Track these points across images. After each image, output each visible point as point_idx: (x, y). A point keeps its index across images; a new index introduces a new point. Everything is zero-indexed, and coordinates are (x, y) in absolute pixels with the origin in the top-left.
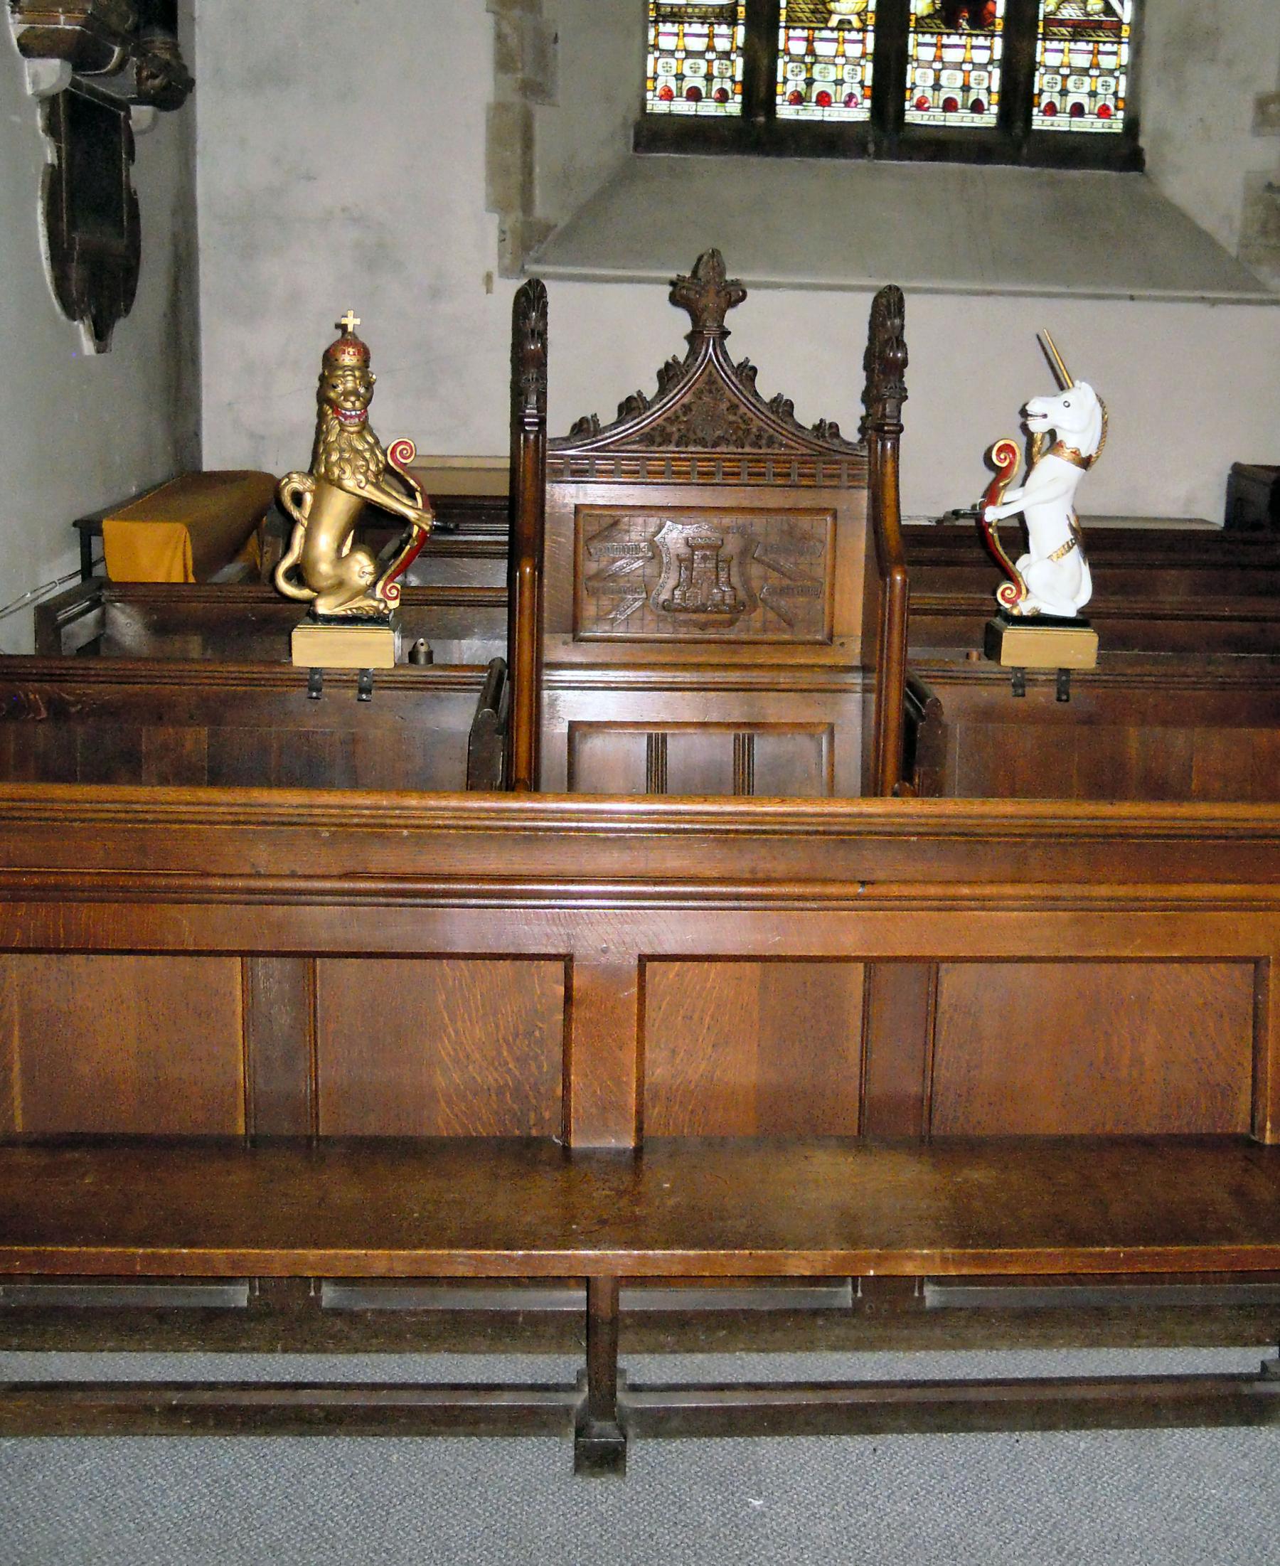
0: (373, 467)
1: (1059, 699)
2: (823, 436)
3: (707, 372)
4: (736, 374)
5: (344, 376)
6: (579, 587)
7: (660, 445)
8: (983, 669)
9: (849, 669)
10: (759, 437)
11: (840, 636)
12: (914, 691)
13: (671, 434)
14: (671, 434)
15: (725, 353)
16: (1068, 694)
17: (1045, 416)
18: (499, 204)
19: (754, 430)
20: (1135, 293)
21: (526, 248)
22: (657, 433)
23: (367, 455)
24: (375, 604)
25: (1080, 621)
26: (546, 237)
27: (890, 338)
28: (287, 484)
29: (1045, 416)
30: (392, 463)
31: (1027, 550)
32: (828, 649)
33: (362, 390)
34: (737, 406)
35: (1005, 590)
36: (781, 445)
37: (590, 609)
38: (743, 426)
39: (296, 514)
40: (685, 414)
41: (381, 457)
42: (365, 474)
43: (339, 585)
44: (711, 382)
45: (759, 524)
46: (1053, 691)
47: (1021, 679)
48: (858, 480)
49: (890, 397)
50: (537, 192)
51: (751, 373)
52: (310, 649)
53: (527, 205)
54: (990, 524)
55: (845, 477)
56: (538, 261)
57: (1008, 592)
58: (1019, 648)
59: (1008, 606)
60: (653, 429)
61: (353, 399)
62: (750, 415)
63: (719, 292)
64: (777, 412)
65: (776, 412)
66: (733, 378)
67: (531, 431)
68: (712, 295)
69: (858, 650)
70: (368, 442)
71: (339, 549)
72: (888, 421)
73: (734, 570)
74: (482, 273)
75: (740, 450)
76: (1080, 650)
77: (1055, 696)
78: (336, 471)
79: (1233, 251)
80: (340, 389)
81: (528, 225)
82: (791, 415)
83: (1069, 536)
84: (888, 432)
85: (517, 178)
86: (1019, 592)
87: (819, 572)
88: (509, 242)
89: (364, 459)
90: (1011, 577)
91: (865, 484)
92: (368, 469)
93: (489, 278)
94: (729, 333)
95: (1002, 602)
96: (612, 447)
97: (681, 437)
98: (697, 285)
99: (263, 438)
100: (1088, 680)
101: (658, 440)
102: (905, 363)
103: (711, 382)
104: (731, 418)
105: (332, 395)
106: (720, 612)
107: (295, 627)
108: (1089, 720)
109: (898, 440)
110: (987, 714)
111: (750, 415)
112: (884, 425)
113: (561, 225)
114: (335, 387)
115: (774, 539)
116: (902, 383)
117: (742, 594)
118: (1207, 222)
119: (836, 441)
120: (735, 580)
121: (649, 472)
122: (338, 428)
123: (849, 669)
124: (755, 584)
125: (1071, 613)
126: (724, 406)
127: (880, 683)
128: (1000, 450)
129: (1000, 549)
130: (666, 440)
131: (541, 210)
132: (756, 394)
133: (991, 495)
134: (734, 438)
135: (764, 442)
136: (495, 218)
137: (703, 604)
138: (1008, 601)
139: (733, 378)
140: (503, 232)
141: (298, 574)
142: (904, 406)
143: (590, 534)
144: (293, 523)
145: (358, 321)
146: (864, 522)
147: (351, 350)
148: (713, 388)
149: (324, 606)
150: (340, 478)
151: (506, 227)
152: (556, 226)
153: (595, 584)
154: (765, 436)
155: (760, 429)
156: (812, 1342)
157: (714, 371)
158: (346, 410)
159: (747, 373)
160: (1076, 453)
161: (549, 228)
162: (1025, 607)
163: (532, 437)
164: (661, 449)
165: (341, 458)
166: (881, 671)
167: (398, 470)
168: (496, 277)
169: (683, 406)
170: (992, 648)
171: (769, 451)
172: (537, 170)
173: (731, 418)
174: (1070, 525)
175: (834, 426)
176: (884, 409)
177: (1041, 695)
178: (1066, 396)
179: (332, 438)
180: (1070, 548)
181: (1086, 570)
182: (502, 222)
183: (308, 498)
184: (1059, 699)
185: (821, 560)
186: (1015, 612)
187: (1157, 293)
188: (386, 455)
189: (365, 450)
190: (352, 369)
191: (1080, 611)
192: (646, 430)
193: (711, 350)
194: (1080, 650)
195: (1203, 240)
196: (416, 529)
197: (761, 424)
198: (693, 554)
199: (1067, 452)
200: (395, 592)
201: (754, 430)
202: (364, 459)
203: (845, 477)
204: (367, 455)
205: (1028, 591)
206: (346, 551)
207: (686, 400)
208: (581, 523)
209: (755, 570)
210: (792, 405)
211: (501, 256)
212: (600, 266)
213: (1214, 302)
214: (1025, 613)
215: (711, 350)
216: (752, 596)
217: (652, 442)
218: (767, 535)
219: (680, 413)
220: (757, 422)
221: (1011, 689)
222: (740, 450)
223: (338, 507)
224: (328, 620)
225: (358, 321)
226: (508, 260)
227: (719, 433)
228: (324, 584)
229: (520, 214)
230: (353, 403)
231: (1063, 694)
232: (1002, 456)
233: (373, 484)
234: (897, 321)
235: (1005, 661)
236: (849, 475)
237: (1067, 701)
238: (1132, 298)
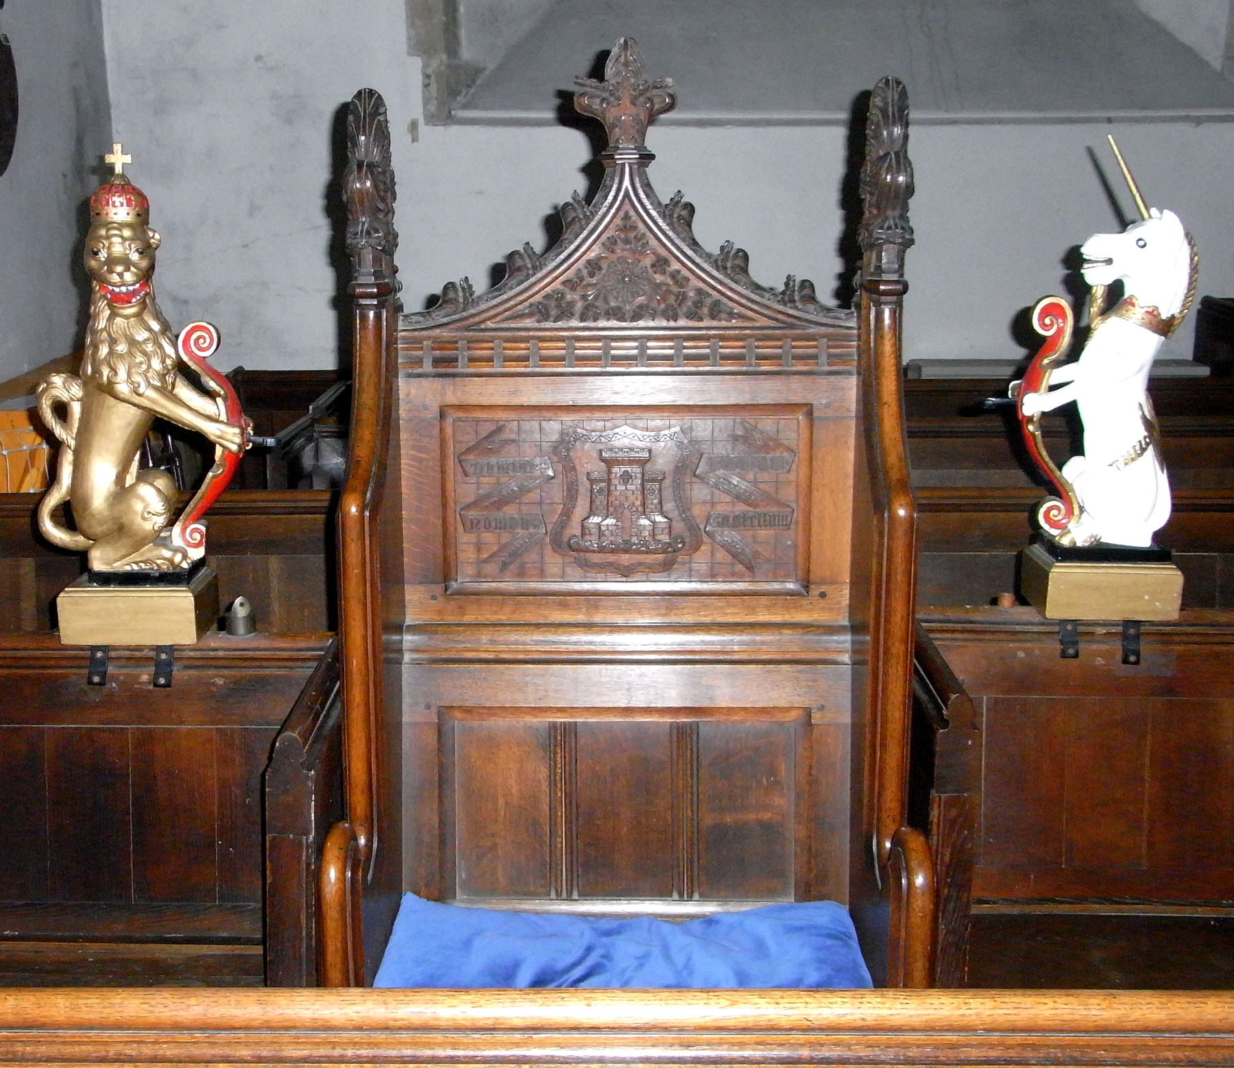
0: (156, 364)
1: (1125, 661)
2: (793, 301)
3: (621, 214)
4: (664, 217)
5: (108, 237)
6: (451, 519)
7: (556, 320)
8: (1016, 618)
9: (832, 630)
10: (698, 304)
11: (823, 582)
12: (927, 666)
13: (572, 304)
14: (572, 304)
15: (647, 186)
16: (1137, 654)
17: (1109, 261)
18: (420, 47)
19: (691, 294)
20: (1112, 114)
21: (453, 93)
22: (553, 304)
23: (149, 347)
24: (167, 553)
25: (1162, 549)
26: (474, 81)
27: (887, 154)
28: (45, 390)
29: (1109, 261)
30: (185, 358)
31: (1078, 450)
32: (804, 602)
33: (135, 257)
34: (666, 262)
35: (1049, 510)
36: (731, 315)
37: (466, 554)
38: (675, 289)
39: (59, 431)
40: (592, 275)
41: (170, 350)
42: (145, 374)
43: (120, 530)
44: (627, 226)
45: (703, 427)
46: (1117, 646)
47: (1072, 634)
48: (844, 363)
49: (888, 241)
50: (463, 33)
51: (684, 213)
52: (86, 618)
53: (452, 46)
54: (1030, 420)
55: (823, 358)
56: (465, 107)
57: (1054, 512)
58: (1072, 592)
59: (1054, 532)
60: (546, 297)
61: (119, 269)
62: (685, 272)
63: (636, 98)
64: (725, 268)
65: (721, 268)
66: (660, 222)
67: (369, 307)
68: (626, 101)
69: (846, 601)
70: (150, 330)
71: (120, 479)
72: (885, 277)
73: (668, 493)
74: (409, 121)
75: (672, 324)
76: (1158, 593)
77: (1119, 657)
78: (106, 372)
79: (1217, 64)
80: (103, 255)
81: (453, 68)
82: (745, 270)
83: (1141, 432)
84: (885, 293)
85: (440, 18)
86: (1070, 512)
87: (788, 494)
88: (434, 86)
89: (145, 353)
90: (1056, 490)
91: (853, 367)
92: (149, 366)
93: (414, 126)
94: (652, 157)
95: (1046, 526)
96: (490, 324)
97: (587, 308)
98: (604, 89)
99: (186, 302)
100: (1163, 633)
101: (554, 312)
102: (910, 190)
103: (627, 226)
104: (659, 278)
105: (93, 263)
106: (649, 552)
107: (62, 590)
108: (1168, 688)
109: (899, 304)
110: (1022, 681)
111: (685, 272)
112: (878, 282)
113: (491, 66)
114: (96, 253)
115: (722, 449)
116: (907, 220)
117: (679, 526)
118: (1188, 36)
119: (811, 307)
120: (669, 506)
121: (543, 359)
122: (107, 312)
123: (832, 630)
124: (698, 511)
125: (1143, 541)
126: (648, 261)
127: (876, 641)
128: (1046, 312)
129: (1044, 453)
130: (565, 312)
131: (467, 53)
132: (694, 244)
133: (1026, 372)
134: (663, 306)
135: (705, 310)
136: (417, 63)
137: (626, 542)
138: (1055, 525)
139: (660, 222)
140: (427, 76)
141: (67, 515)
142: (910, 254)
143: (464, 447)
144: (56, 446)
145: (128, 159)
146: (853, 423)
147: (117, 200)
148: (632, 235)
149: (99, 561)
150: (111, 383)
151: (430, 71)
152: (484, 69)
153: (472, 514)
154: (709, 301)
155: (699, 292)
156: (754, 609)
157: (632, 213)
158: (114, 285)
159: (681, 214)
160: (1153, 313)
161: (478, 71)
162: (1078, 534)
163: (371, 314)
164: (559, 324)
165: (111, 352)
166: (877, 631)
167: (193, 366)
168: (423, 128)
169: (589, 262)
170: (1029, 589)
171: (715, 323)
172: (462, 9)
173: (659, 278)
174: (1144, 417)
175: (807, 285)
176: (879, 259)
177: (1101, 655)
178: (1133, 233)
179: (102, 324)
180: (1143, 450)
181: (1163, 479)
182: (425, 66)
183: (76, 409)
184: (1125, 661)
185: (792, 476)
186: (1065, 542)
187: (1138, 114)
188: (175, 346)
189: (146, 341)
190: (122, 226)
191: (1157, 536)
192: (538, 298)
193: (627, 183)
194: (1158, 593)
195: (1189, 56)
196: (219, 451)
197: (701, 285)
198: (609, 472)
199: (1137, 313)
200: (198, 536)
201: (691, 294)
202: (145, 353)
203: (823, 358)
204: (149, 347)
205: (1082, 510)
206: (130, 479)
207: (591, 255)
208: (449, 431)
209: (699, 493)
210: (746, 257)
211: (426, 101)
212: (527, 109)
213: (1198, 121)
214: (1079, 544)
215: (627, 183)
216: (692, 527)
217: (546, 317)
218: (713, 441)
219: (585, 272)
220: (695, 282)
221: (1059, 647)
222: (672, 324)
223: (119, 423)
224: (107, 579)
225: (128, 159)
226: (433, 108)
227: (641, 299)
228: (98, 529)
229: (444, 57)
230: (121, 275)
231: (1130, 656)
232: (1047, 321)
233: (155, 388)
234: (897, 131)
235: (1052, 612)
236: (830, 356)
237: (1137, 663)
238: (1109, 120)
